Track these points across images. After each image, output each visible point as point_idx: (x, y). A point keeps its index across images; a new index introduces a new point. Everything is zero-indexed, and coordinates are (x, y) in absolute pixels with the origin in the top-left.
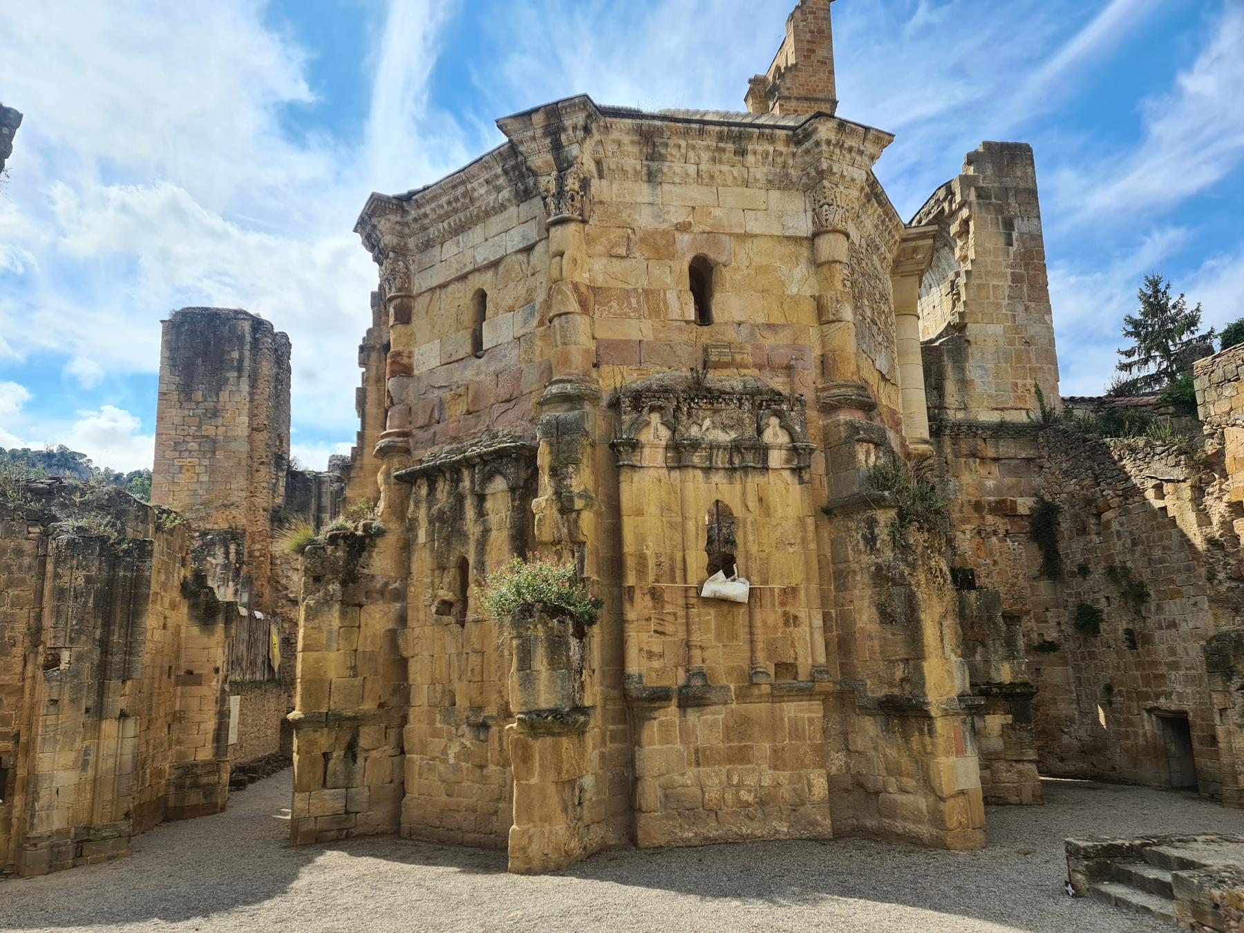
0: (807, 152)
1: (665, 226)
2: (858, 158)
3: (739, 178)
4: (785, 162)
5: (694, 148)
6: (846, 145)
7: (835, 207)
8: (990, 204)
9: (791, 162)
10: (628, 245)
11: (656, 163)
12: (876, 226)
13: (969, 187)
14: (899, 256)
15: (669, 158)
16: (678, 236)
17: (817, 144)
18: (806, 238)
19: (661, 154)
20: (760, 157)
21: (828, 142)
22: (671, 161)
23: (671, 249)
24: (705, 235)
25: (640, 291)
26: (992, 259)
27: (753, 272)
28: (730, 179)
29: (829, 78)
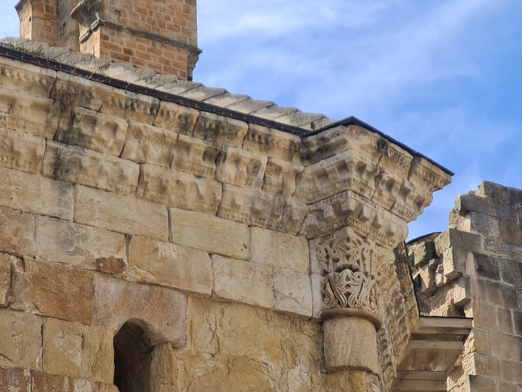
0: (323, 175)
1: (78, 261)
2: (400, 200)
3: (208, 200)
4: (283, 185)
5: (138, 134)
6: (385, 177)
7: (363, 276)
8: (497, 285)
9: (292, 186)
10: (11, 286)
11: (71, 149)
12: (388, 310)
13: (465, 252)
14: (405, 362)
15: (95, 144)
16: (99, 280)
17: (344, 166)
18: (310, 319)
19: (81, 135)
20: (245, 169)
21: (361, 168)
22: (97, 150)
23: (87, 303)
24: (145, 288)
25: (27, 374)
26: (502, 379)
27: (222, 366)
28: (191, 196)
29: (187, 11)
